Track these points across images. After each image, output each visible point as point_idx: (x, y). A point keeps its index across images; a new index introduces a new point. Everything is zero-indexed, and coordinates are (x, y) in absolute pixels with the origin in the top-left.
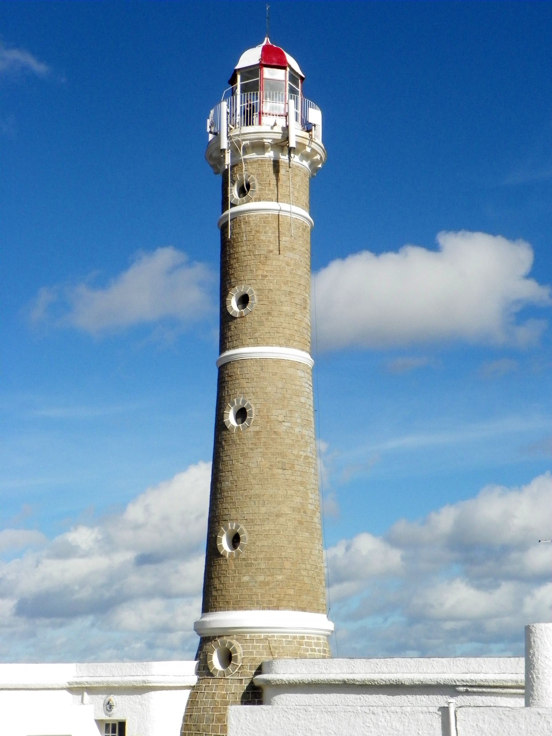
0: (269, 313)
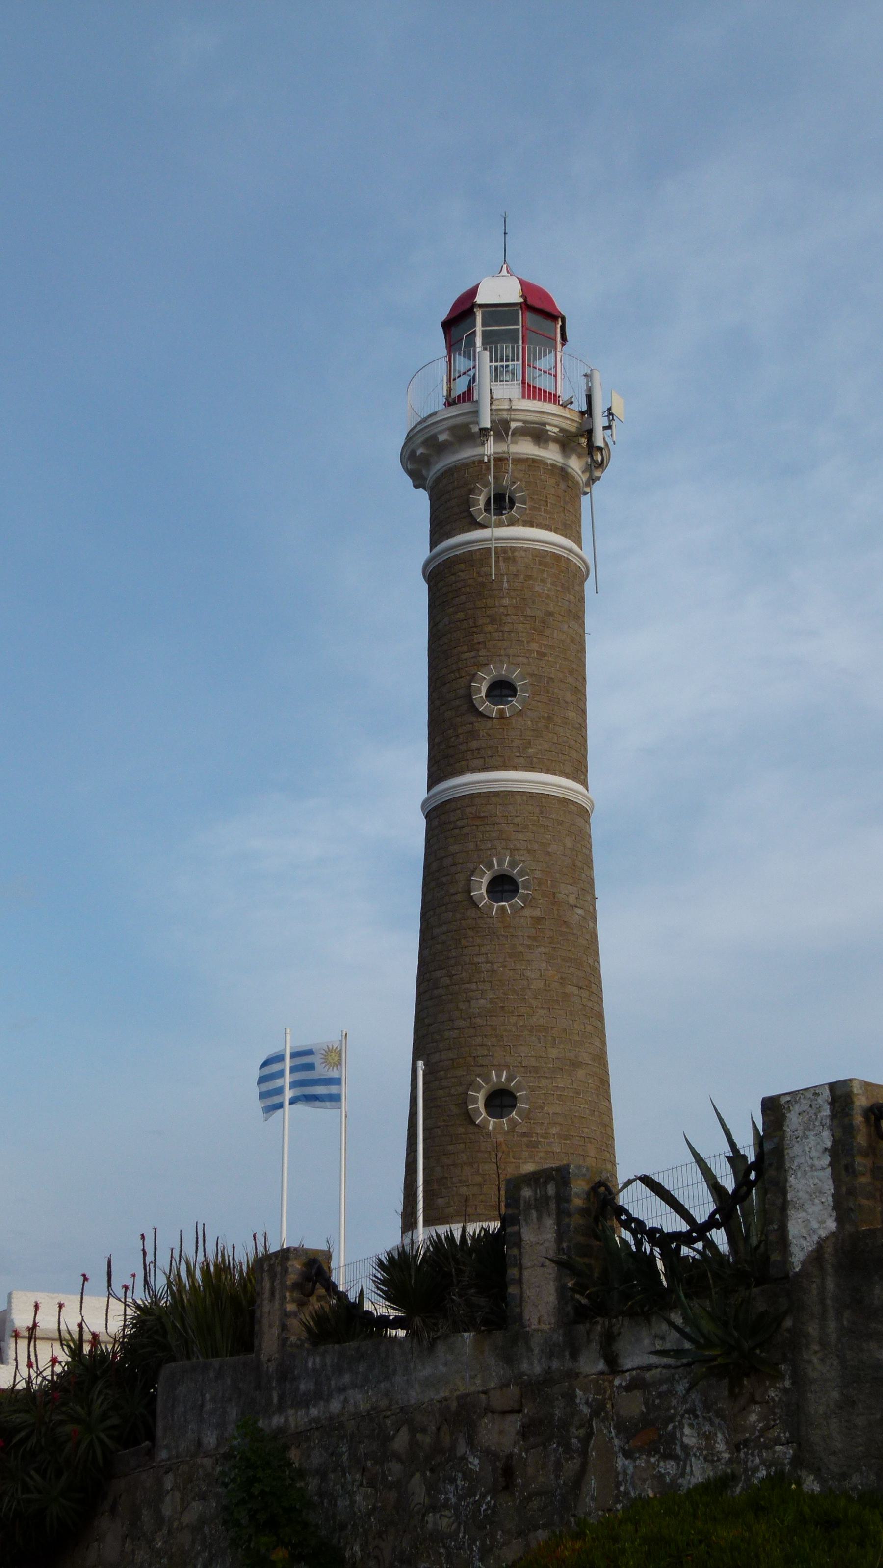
0: (549, 718)
